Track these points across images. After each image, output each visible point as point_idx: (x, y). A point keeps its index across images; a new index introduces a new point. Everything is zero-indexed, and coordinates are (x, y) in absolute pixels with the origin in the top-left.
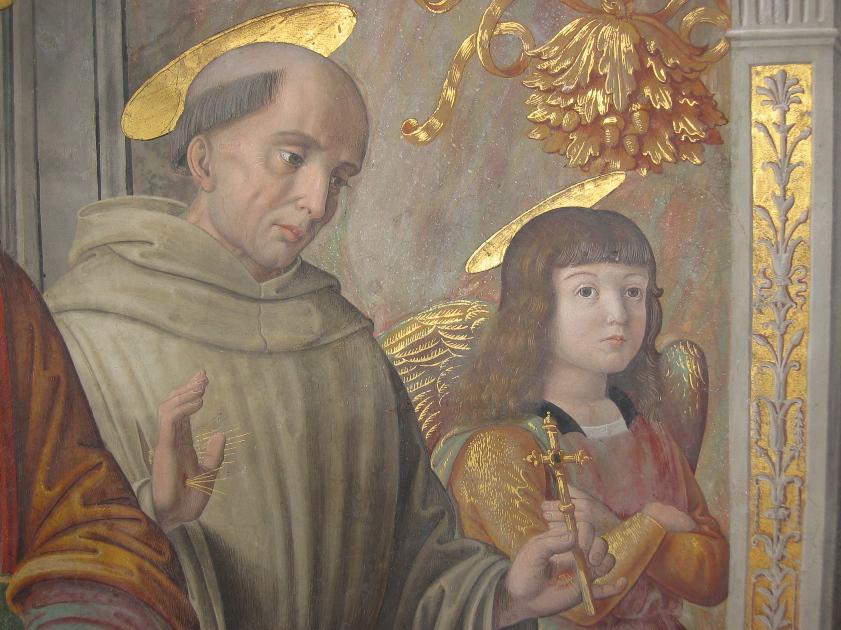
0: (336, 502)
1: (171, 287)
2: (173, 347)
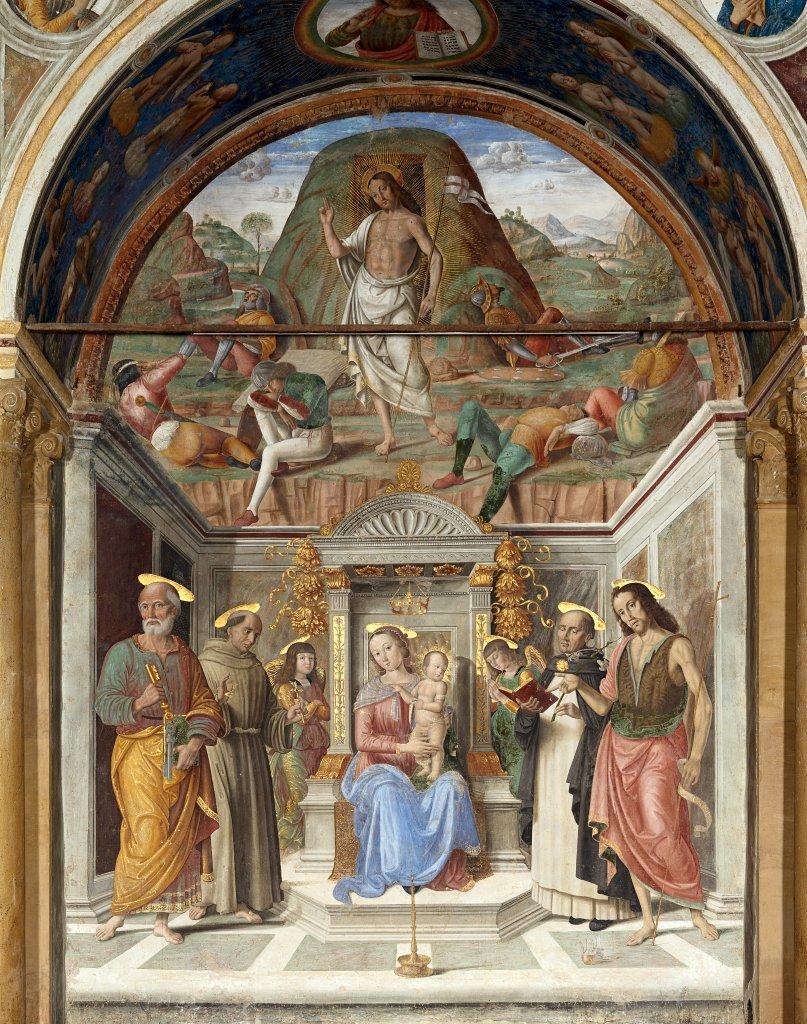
0: (254, 699)
1: (223, 656)
2: (223, 667)
